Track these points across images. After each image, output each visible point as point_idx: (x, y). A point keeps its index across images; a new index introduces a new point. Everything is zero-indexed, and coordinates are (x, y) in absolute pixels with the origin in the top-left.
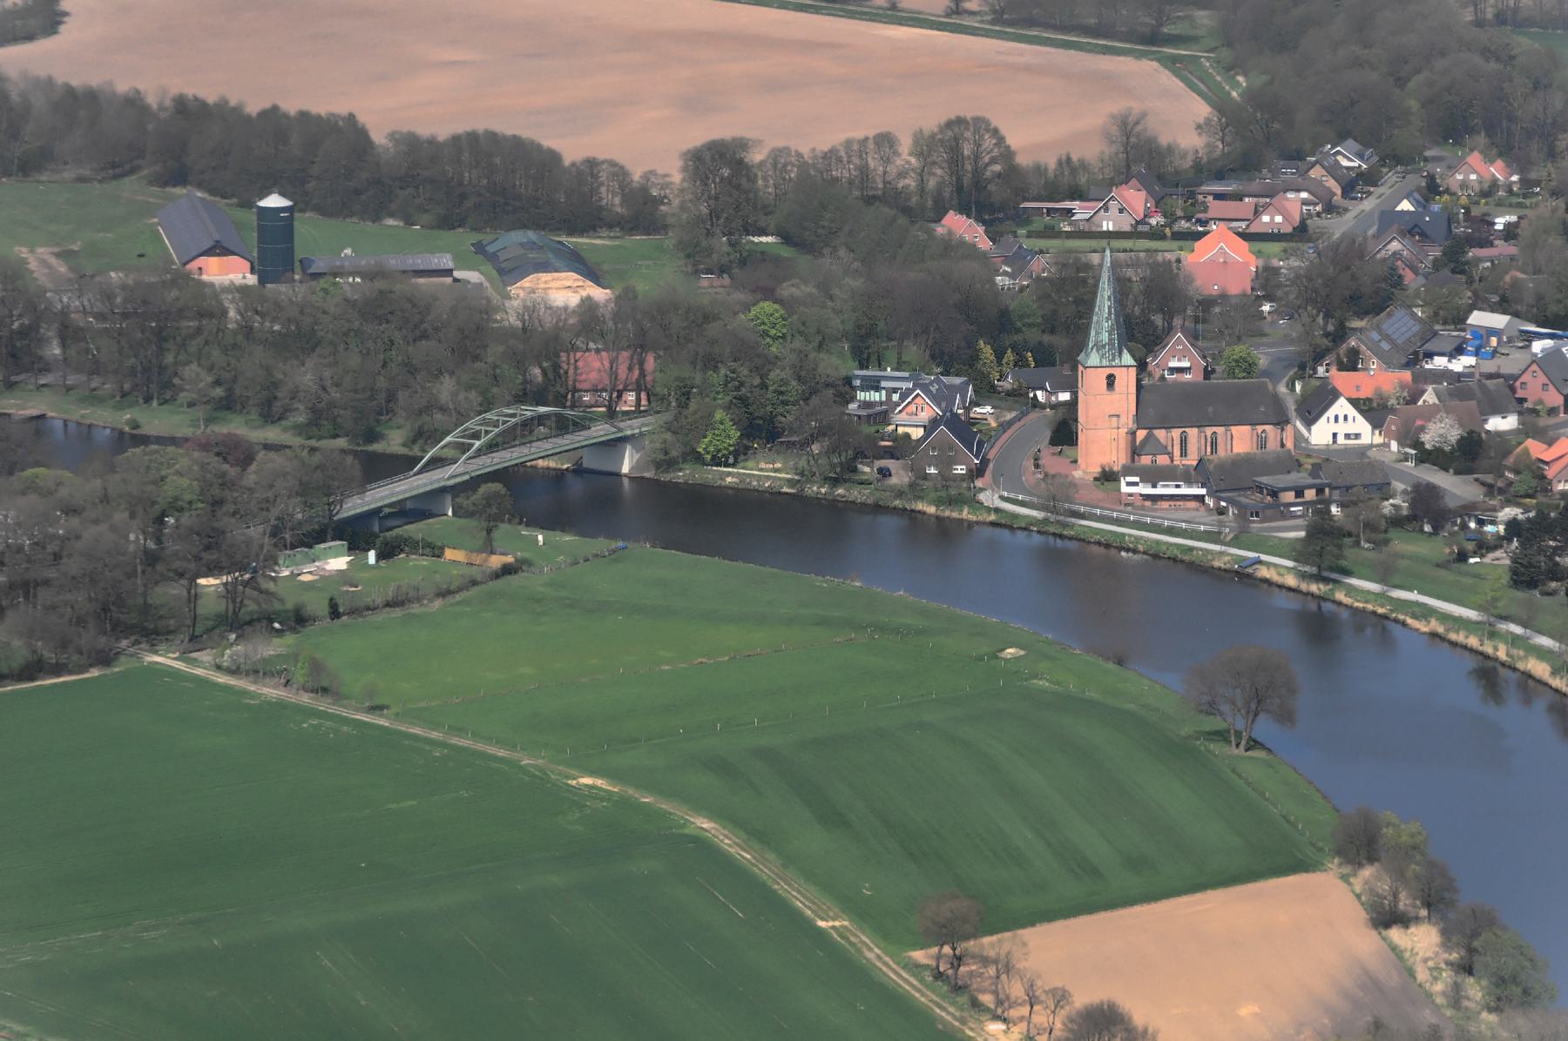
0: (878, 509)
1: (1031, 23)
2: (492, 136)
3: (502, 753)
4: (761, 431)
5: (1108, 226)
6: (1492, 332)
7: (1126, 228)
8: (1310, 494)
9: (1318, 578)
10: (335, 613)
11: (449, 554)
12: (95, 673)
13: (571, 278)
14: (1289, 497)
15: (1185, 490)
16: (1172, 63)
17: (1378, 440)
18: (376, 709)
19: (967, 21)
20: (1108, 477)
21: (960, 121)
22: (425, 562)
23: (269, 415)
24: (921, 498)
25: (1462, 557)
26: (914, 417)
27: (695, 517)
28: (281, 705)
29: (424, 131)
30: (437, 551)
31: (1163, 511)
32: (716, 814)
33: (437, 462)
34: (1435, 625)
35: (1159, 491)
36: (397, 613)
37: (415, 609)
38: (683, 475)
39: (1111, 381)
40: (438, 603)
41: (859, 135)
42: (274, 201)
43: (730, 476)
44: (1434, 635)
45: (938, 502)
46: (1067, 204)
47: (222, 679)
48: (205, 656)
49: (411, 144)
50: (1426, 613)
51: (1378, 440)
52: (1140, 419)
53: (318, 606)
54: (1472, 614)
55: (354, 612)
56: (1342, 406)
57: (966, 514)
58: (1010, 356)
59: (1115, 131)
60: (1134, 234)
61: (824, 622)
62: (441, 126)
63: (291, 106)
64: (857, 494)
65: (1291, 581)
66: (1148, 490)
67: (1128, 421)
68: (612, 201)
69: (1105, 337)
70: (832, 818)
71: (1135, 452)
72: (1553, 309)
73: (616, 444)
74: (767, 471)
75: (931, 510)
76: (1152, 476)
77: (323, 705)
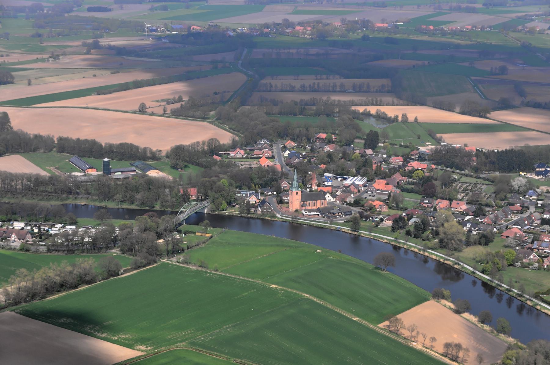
0: (258, 218)
1: (180, 116)
2: (126, 144)
3: (230, 276)
4: (229, 204)
5: (238, 157)
6: (329, 177)
7: (241, 157)
8: (340, 214)
9: (355, 231)
10: (188, 249)
11: (197, 234)
12: (155, 265)
13: (157, 171)
14: (337, 214)
15: (316, 213)
16: (209, 122)
17: (334, 200)
18: (217, 271)
19: (167, 115)
20: (297, 211)
21: (212, 139)
22: (193, 235)
23: (132, 203)
24: (266, 216)
25: (377, 226)
26: (253, 200)
27: (218, 221)
28: (197, 270)
30: (195, 233)
31: (310, 215)
32: (307, 293)
33: (182, 212)
34: (385, 241)
35: (311, 214)
36: (198, 247)
37: (200, 246)
38: (217, 213)
39: (297, 193)
40: (203, 245)
42: (106, 159)
44: (386, 243)
45: (269, 217)
46: (228, 152)
47: (181, 265)
48: (174, 259)
49: (111, 146)
50: (382, 238)
51: (334, 200)
52: (302, 200)
53: (185, 247)
54: (393, 239)
55: (191, 248)
57: (276, 219)
58: (257, 186)
59: (231, 139)
61: (278, 245)
62: (116, 141)
63: (82, 138)
64: (252, 216)
65: (350, 232)
66: (309, 214)
67: (300, 201)
68: (149, 154)
69: (296, 186)
70: (330, 294)
71: (302, 206)
72: (339, 172)
73: (204, 208)
74: (233, 211)
75: (269, 219)
76: (310, 211)
77: (204, 270)
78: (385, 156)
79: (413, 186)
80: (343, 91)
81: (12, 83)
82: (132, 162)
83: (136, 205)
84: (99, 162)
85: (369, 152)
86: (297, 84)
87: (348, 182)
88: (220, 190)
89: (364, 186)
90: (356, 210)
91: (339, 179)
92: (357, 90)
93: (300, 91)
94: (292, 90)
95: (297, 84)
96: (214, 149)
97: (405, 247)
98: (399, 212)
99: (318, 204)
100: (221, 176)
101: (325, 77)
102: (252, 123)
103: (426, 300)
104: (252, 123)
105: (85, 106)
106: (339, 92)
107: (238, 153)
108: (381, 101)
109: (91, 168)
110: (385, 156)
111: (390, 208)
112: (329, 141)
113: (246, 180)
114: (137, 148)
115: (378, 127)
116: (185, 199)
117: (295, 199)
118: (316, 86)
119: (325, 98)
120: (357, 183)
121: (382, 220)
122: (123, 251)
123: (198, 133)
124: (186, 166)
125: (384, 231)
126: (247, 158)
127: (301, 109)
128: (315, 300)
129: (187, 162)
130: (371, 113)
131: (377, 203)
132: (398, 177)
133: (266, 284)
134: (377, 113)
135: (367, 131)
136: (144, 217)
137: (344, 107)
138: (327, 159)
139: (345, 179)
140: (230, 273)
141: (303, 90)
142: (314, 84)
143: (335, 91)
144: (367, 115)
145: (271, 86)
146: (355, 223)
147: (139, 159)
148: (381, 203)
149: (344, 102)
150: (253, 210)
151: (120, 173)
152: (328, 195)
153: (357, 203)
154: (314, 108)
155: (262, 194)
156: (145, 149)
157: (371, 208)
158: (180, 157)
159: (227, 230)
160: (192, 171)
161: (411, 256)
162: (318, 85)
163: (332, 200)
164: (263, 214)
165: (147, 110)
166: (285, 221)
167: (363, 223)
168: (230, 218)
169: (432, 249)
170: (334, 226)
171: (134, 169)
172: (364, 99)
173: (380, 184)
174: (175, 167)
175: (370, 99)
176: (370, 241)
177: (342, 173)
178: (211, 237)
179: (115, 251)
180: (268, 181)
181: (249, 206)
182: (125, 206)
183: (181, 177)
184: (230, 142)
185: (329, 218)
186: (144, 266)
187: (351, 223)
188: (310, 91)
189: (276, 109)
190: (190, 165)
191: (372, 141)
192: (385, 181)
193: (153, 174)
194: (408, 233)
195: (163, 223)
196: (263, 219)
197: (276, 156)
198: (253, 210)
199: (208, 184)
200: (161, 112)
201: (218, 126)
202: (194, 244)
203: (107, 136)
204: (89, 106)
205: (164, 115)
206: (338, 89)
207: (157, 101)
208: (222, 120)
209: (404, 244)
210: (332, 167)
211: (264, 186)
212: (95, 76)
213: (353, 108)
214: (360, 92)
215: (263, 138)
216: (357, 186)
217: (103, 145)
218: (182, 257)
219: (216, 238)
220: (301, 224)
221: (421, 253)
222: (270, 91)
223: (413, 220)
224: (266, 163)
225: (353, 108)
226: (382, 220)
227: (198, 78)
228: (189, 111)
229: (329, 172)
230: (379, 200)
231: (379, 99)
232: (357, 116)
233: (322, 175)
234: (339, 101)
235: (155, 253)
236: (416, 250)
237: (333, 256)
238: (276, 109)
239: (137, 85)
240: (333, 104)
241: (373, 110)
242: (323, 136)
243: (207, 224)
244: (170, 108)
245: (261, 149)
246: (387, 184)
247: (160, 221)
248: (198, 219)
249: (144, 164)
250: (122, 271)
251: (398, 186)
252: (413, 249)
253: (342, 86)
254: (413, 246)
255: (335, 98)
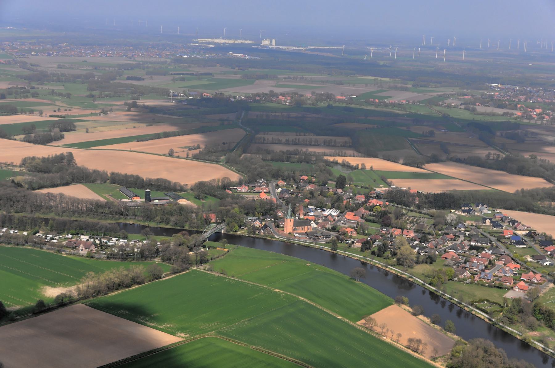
11: (217, 249)
12: (188, 271)
13: (185, 200)
16: (221, 165)
20: (290, 233)
22: (214, 250)
23: (168, 224)
26: (257, 224)
27: (232, 239)
28: (219, 276)
29: (139, 175)
30: (216, 248)
31: (299, 236)
33: (205, 232)
38: (231, 233)
40: (223, 257)
41: (100, 168)
42: (148, 190)
43: (238, 233)
49: (150, 180)
50: (354, 256)
52: (294, 226)
56: (312, 222)
60: (247, 192)
61: (278, 259)
62: (154, 177)
63: (129, 174)
64: (257, 236)
67: (292, 226)
68: (178, 187)
70: (319, 297)
71: (294, 230)
72: (319, 205)
74: (242, 232)
76: (300, 234)
77: (225, 276)
78: (351, 194)
79: (374, 218)
80: (317, 145)
81: (74, 130)
82: (166, 193)
83: (172, 225)
84: (142, 192)
85: (340, 191)
86: (283, 139)
87: (326, 213)
88: (234, 216)
89: (338, 216)
90: (333, 234)
91: (319, 211)
92: (327, 145)
93: (286, 144)
94: (279, 143)
95: (283, 139)
96: (226, 185)
97: (372, 263)
98: (366, 237)
99: (306, 229)
100: (234, 206)
101: (302, 134)
102: (253, 166)
103: (390, 304)
104: (253, 166)
105: (129, 149)
106: (314, 145)
107: (243, 189)
108: (345, 153)
109: (136, 196)
110: (351, 194)
111: (358, 233)
112: (310, 182)
113: (250, 209)
114: (169, 182)
115: (345, 173)
116: (207, 222)
117: (289, 225)
118: (297, 141)
119: (304, 150)
120: (333, 214)
121: (353, 242)
122: (163, 260)
123: (214, 173)
124: (206, 197)
125: (355, 251)
126: (250, 192)
127: (287, 157)
128: (309, 302)
129: (207, 194)
130: (338, 162)
131: (349, 230)
132: (362, 210)
133: (272, 289)
134: (343, 162)
135: (338, 175)
136: (178, 235)
137: (319, 157)
138: (309, 195)
139: (324, 211)
140: (244, 280)
141: (287, 143)
142: (296, 139)
143: (311, 145)
144: (336, 163)
145: (264, 139)
146: (334, 244)
147: (171, 190)
148: (352, 230)
149: (319, 153)
150: (257, 232)
151: (157, 201)
152: (312, 222)
153: (334, 229)
154: (297, 156)
155: (264, 220)
156: (175, 183)
157: (344, 234)
158: (202, 190)
159: (239, 246)
160: (211, 201)
161: (375, 270)
162: (299, 140)
163: (316, 226)
164: (265, 235)
165: (174, 154)
166: (281, 241)
167: (339, 245)
168: (240, 237)
169: (391, 265)
170: (318, 246)
171: (168, 198)
172: (333, 151)
173: (349, 215)
174: (198, 197)
175: (337, 151)
176: (345, 257)
177: (321, 206)
178: (228, 251)
179: (157, 260)
180: (267, 210)
181: (255, 229)
182: (163, 226)
183: (203, 205)
184: (238, 180)
185: (314, 239)
186: (180, 272)
187: (330, 244)
188: (292, 144)
189: (269, 157)
190: (208, 196)
191: (341, 183)
192: (353, 213)
193: (183, 202)
194: (373, 253)
195: (192, 240)
196: (265, 239)
197: (271, 192)
198: (257, 232)
199: (225, 211)
200: (185, 156)
201: (227, 168)
202: (216, 256)
203: (148, 172)
204: (132, 149)
205: (187, 158)
206: (313, 143)
207: (182, 148)
208: (230, 163)
209: (370, 261)
210: (313, 201)
211: (265, 214)
212: (134, 127)
213: (326, 158)
214: (328, 146)
215: (261, 178)
216: (333, 216)
217: (145, 179)
218: (207, 266)
219: (232, 252)
220: (293, 243)
221: (384, 268)
222: (263, 143)
223: (376, 243)
224: (264, 197)
225: (326, 158)
226: (353, 242)
227: (210, 131)
228: (206, 156)
229: (311, 205)
230: (350, 227)
231: (344, 152)
232: (328, 163)
233: (306, 207)
234: (315, 152)
235: (187, 262)
236: (380, 266)
237: (319, 268)
238: (269, 157)
239: (167, 135)
240: (310, 155)
241: (340, 160)
242: (305, 178)
243: (225, 241)
244: (191, 153)
245: (260, 186)
246: (355, 215)
247: (190, 238)
248: (217, 237)
249: (175, 194)
250: (163, 275)
251: (363, 217)
252: (377, 265)
253: (316, 141)
254: (377, 262)
255: (312, 150)
